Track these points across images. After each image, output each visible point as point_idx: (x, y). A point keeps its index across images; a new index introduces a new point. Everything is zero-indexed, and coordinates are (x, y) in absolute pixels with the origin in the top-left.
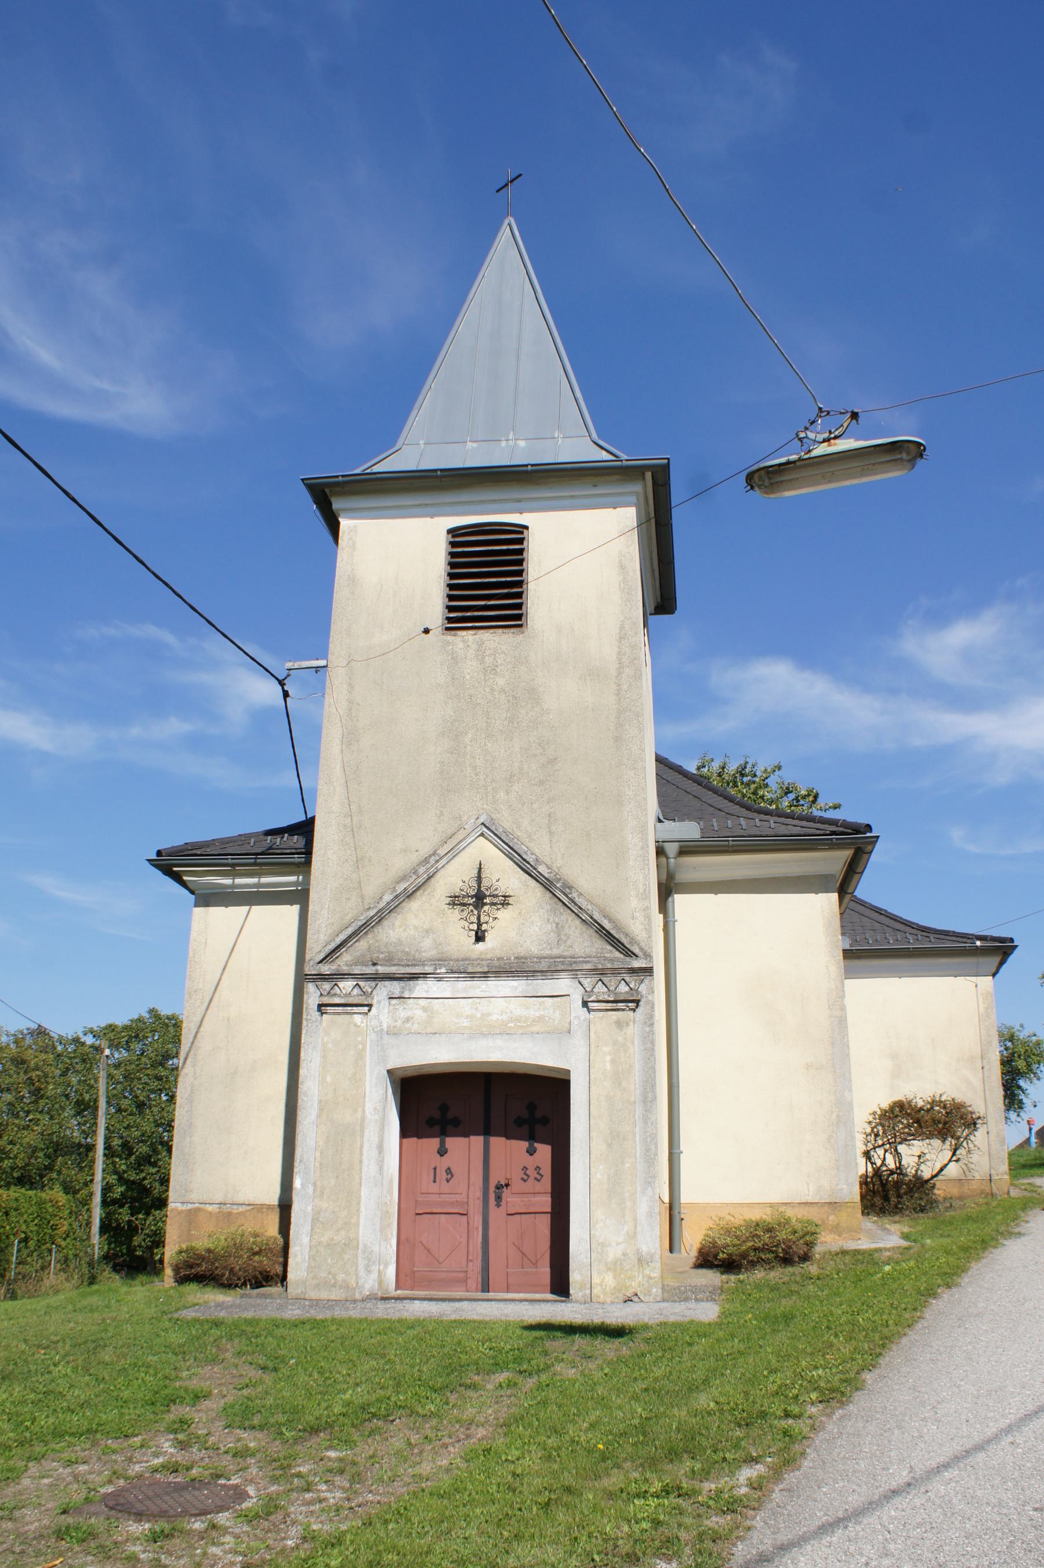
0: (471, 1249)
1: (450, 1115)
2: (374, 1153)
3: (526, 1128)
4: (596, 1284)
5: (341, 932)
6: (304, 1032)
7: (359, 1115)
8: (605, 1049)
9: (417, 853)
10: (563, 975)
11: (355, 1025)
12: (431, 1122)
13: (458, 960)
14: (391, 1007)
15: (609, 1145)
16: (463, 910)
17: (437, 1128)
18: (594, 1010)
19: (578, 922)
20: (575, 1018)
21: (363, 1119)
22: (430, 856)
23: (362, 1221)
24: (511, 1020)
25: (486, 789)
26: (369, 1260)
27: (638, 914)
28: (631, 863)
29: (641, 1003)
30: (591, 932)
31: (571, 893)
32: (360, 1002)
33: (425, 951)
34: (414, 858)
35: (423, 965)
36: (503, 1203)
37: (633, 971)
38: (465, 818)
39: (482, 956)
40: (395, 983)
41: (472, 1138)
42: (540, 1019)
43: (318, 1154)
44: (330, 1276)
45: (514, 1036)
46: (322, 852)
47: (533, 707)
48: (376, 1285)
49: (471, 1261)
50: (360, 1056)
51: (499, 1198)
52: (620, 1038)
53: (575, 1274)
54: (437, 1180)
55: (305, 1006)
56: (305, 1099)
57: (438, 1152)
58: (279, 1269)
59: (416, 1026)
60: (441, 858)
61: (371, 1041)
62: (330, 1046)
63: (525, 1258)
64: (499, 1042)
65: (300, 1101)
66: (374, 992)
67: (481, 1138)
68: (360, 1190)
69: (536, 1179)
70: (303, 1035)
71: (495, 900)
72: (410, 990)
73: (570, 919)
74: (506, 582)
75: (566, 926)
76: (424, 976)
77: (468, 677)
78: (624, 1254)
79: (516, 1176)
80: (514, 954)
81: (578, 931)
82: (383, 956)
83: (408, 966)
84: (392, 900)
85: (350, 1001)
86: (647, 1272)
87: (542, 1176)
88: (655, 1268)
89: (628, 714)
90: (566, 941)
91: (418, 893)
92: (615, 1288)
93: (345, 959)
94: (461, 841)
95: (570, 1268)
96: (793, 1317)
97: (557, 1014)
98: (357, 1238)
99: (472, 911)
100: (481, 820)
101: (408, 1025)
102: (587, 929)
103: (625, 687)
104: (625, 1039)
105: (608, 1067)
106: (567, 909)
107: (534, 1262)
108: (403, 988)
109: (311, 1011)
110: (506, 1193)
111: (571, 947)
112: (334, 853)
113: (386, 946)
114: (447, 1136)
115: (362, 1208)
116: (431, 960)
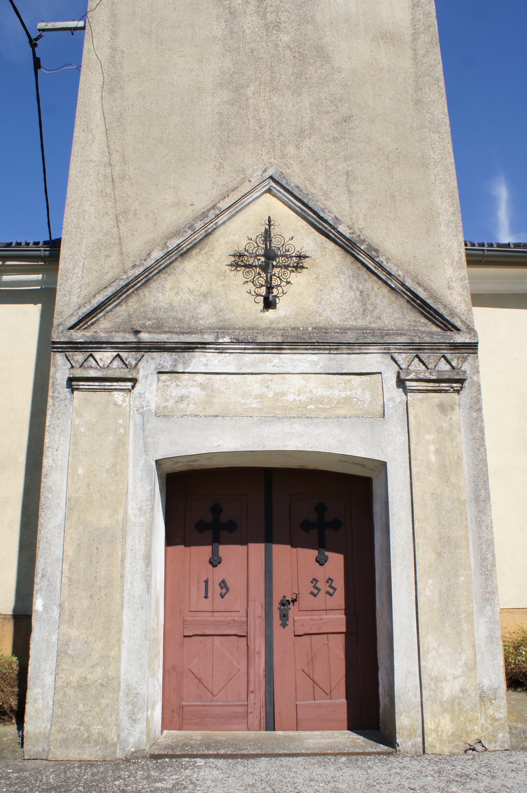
0: (251, 678)
1: (224, 518)
2: (140, 565)
3: (209, 533)
4: (430, 729)
5: (99, 293)
6: (49, 412)
7: (120, 517)
8: (427, 437)
10: (373, 349)
11: (115, 404)
12: (201, 526)
13: (243, 329)
14: (161, 384)
15: (439, 554)
16: (248, 272)
17: (209, 533)
18: (413, 391)
19: (385, 290)
20: (389, 399)
21: (125, 521)
22: (209, 210)
23: (124, 654)
24: (311, 401)
25: (273, 142)
26: (134, 705)
27: (454, 284)
28: (443, 229)
29: (466, 384)
30: (401, 302)
31: (378, 257)
32: (122, 375)
33: (202, 319)
34: (188, 213)
35: (202, 332)
36: (290, 622)
37: (455, 347)
38: (249, 172)
39: (274, 326)
40: (166, 355)
41: (252, 546)
42: (347, 400)
43: (66, 567)
44: (82, 728)
45: (316, 420)
46: (77, 204)
47: (322, 65)
48: (144, 739)
49: (252, 692)
50: (122, 442)
51: (284, 616)
52: (444, 425)
53: (402, 718)
54: (210, 595)
55: (51, 381)
56: (50, 496)
57: (210, 562)
58: (14, 703)
59: (192, 407)
60: (222, 212)
61: (135, 425)
62: (82, 430)
63: (316, 687)
64: (298, 427)
65: (42, 498)
66: (140, 365)
67: (262, 545)
68: (120, 614)
69: (328, 593)
70: (48, 417)
71: (288, 262)
72: (184, 363)
73: (376, 286)
75: (373, 295)
76: (202, 346)
77: (248, 32)
78: (463, 691)
79: (306, 588)
81: (386, 300)
82: (150, 322)
83: (183, 333)
84: (163, 258)
85: (110, 374)
86: (490, 712)
87: (335, 589)
88: (499, 706)
89: (427, 78)
90: (373, 311)
91: (194, 252)
92: (453, 734)
93: (102, 326)
94: (245, 195)
95: (396, 710)
97: (367, 396)
98: (118, 677)
100: (270, 173)
101: (182, 406)
102: (397, 298)
103: (421, 52)
104: (451, 425)
105: (433, 458)
106: (372, 275)
107: (328, 691)
108: (175, 361)
109: (59, 388)
110: (293, 610)
111: (379, 318)
112: (91, 205)
113: (154, 311)
114: (220, 544)
115: (125, 637)
116: (210, 329)
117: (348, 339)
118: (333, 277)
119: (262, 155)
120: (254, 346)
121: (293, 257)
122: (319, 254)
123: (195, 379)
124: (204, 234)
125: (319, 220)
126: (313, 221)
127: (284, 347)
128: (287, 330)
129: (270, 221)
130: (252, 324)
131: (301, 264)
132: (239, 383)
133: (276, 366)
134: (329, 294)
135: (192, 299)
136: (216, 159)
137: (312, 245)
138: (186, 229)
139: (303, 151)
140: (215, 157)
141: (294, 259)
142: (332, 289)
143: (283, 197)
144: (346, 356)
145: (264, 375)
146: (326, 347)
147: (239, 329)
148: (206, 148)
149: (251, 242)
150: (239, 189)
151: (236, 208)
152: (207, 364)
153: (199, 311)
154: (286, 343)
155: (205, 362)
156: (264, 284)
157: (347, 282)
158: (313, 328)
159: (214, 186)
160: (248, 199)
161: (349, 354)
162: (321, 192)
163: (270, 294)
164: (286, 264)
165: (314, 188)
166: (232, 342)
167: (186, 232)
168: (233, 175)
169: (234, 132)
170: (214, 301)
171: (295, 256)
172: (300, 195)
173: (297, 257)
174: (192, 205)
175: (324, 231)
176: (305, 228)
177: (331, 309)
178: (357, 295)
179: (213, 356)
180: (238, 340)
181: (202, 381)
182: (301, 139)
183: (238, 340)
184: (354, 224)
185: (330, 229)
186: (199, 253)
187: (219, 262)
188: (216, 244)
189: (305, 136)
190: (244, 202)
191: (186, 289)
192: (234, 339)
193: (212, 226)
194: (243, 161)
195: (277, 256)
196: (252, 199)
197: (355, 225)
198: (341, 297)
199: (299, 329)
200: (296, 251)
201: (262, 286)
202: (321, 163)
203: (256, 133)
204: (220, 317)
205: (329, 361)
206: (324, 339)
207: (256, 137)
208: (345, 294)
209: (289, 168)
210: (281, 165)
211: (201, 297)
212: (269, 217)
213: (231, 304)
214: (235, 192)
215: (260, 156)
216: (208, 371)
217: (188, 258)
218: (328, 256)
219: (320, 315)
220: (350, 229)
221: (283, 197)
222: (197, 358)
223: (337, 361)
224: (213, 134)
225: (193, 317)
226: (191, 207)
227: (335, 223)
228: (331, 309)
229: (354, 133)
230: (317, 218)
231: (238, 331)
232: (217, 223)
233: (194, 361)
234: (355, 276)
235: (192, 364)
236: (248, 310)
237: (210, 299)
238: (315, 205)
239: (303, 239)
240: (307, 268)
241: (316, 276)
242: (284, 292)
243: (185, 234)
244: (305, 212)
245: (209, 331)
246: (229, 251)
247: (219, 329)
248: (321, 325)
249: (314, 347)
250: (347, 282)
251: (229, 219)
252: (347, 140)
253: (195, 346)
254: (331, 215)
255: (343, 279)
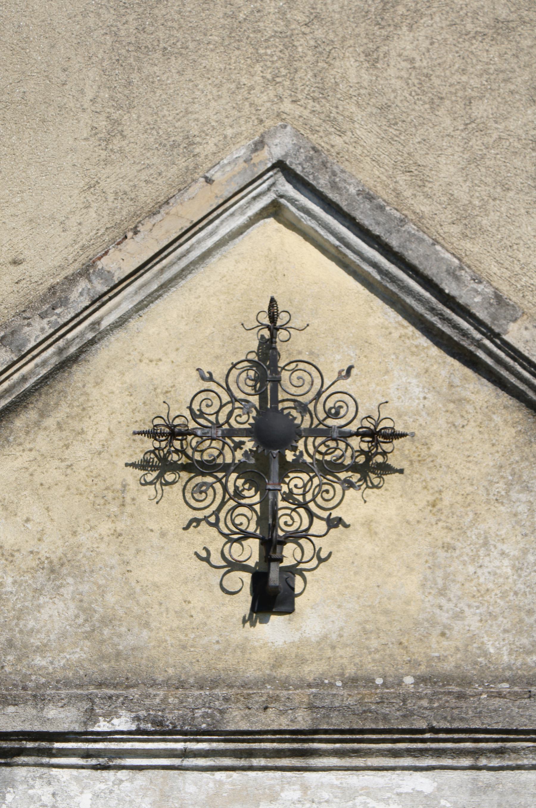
9: (16, 272)
13: (182, 685)
16: (200, 489)
23: (14, 396)
33: (41, 649)
39: (285, 671)
80: (414, 663)
96: (82, 93)
99: (238, 494)
116: (67, 684)
118: (488, 502)
119: (252, 88)
120: (215, 745)
122: (442, 421)
124: (55, 361)
125: (440, 306)
126: (420, 309)
127: (316, 745)
128: (332, 685)
129: (273, 316)
130: (209, 668)
131: (379, 459)
134: (474, 559)
135: (10, 580)
137: (417, 391)
139: (392, 71)
140: (93, 101)
141: (355, 442)
142: (486, 544)
143: (322, 232)
146: (462, 745)
147: (167, 683)
148: (64, 70)
151: (162, 271)
153: (31, 624)
154: (326, 732)
156: (252, 528)
158: (421, 680)
159: (91, 198)
160: (204, 239)
162: (448, 212)
164: (328, 458)
165: (427, 196)
166: (139, 732)
168: (155, 160)
170: (85, 588)
171: (357, 434)
172: (378, 224)
173: (363, 435)
174: (15, 262)
175: (457, 344)
176: (396, 335)
177: (482, 610)
180: (161, 723)
182: (384, 33)
185: (478, 336)
186: (37, 424)
187: (105, 455)
188: (95, 393)
189: (397, 19)
190: (188, 251)
192: (145, 720)
194: (187, 112)
196: (216, 238)
198: (517, 570)
199: (369, 681)
201: (247, 535)
202: (451, 112)
204: (102, 642)
205: (472, 794)
206: (453, 719)
207: (232, 30)
209: (342, 133)
210: (315, 121)
211: (41, 576)
212: (273, 301)
213: (142, 599)
214: (158, 217)
215: (244, 92)
218: (471, 429)
219: (443, 634)
221: (322, 232)
222: (22, 787)
223: (501, 794)
224: (91, 20)
225: (10, 643)
226: (12, 268)
227: (494, 318)
228: (482, 610)
230: (433, 300)
231: (161, 693)
232: (98, 322)
236: (199, 617)
237: (70, 580)
238: (427, 257)
239: (387, 372)
240: (401, 471)
241: (431, 498)
242: (323, 555)
244: (394, 279)
245: (63, 692)
246: (138, 417)
247: (100, 685)
248: (448, 666)
249: (420, 745)
253: (16, 745)
254: (480, 288)
255: (522, 508)
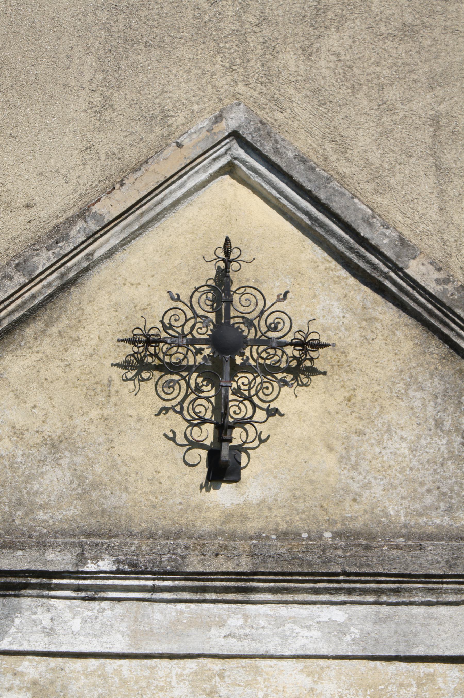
9: (29, 213)
13: (152, 536)
16: (168, 384)
22: (71, 221)
25: (244, 41)
33: (44, 507)
39: (232, 527)
74: (198, 575)
91: (29, 331)
99: (198, 389)
116: (64, 534)
117: (425, 564)
118: (391, 398)
119: (214, 74)
120: (177, 583)
121: (286, 344)
122: (356, 335)
123: (20, 669)
124: (57, 283)
125: (357, 246)
126: (341, 248)
128: (268, 538)
130: (174, 523)
131: (308, 363)
132: (136, 682)
133: (234, 637)
134: (379, 442)
135: (20, 453)
136: (94, 87)
137: (337, 311)
138: (11, 271)
139: (322, 63)
140: (90, 81)
141: (289, 350)
142: (389, 430)
143: (266, 187)
144: (422, 609)
145: (203, 661)
146: (368, 585)
147: (140, 534)
148: (68, 57)
149: (180, 305)
150: (151, 167)
151: (142, 215)
152: (52, 629)
153: (36, 487)
155: (46, 623)
156: (209, 415)
157: (430, 409)
158: (337, 535)
160: (175, 191)
161: (429, 604)
163: (225, 445)
164: (268, 362)
165: (348, 161)
167: (11, 278)
168: (137, 128)
169: (143, 13)
170: (78, 460)
171: (291, 344)
172: (310, 181)
173: (296, 345)
174: (28, 206)
175: (370, 275)
176: (322, 267)
177: (385, 481)
178: (456, 445)
179: (69, 607)
180: (136, 566)
181: (37, 676)
183: (136, 566)
184: (450, 255)
185: (386, 269)
186: (43, 332)
187: (95, 357)
188: (88, 309)
189: (327, 22)
190: (162, 200)
191: (6, 429)
192: (124, 562)
193: (79, 263)
194: (163, 92)
195: (245, 342)
196: (184, 190)
197: (454, 258)
198: (413, 451)
199: (297, 535)
200: (295, 328)
201: (204, 421)
202: (367, 95)
203: (200, 18)
204: (91, 502)
205: (375, 623)
206: (361, 565)
207: (199, 28)
208: (423, 442)
209: (283, 110)
210: (263, 100)
211: (45, 450)
212: (227, 239)
213: (123, 469)
214: (140, 173)
215: (208, 76)
216: (54, 649)
217: (13, 346)
218: (379, 341)
219: (355, 500)
220: (439, 270)
221: (266, 187)
223: (397, 624)
224: (90, 19)
225: (20, 502)
226: (25, 210)
227: (398, 256)
228: (385, 481)
229: (458, 12)
230: (352, 241)
231: (136, 542)
232: (91, 254)
233: (17, 621)
234: (451, 393)
235: (13, 630)
236: (166, 484)
237: (67, 454)
238: (347, 208)
239: (315, 296)
240: (325, 373)
241: (347, 395)
243: (7, 282)
244: (321, 225)
245: (60, 541)
246: (122, 328)
247: (89, 535)
248: (358, 525)
249: (335, 585)
250: (430, 409)
251: (124, 243)
252: (437, 32)
253: (23, 581)
254: (388, 232)
255: (417, 403)
